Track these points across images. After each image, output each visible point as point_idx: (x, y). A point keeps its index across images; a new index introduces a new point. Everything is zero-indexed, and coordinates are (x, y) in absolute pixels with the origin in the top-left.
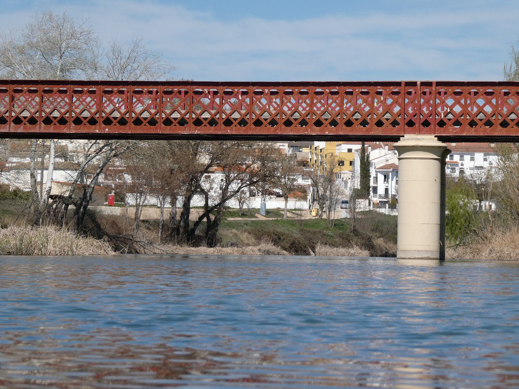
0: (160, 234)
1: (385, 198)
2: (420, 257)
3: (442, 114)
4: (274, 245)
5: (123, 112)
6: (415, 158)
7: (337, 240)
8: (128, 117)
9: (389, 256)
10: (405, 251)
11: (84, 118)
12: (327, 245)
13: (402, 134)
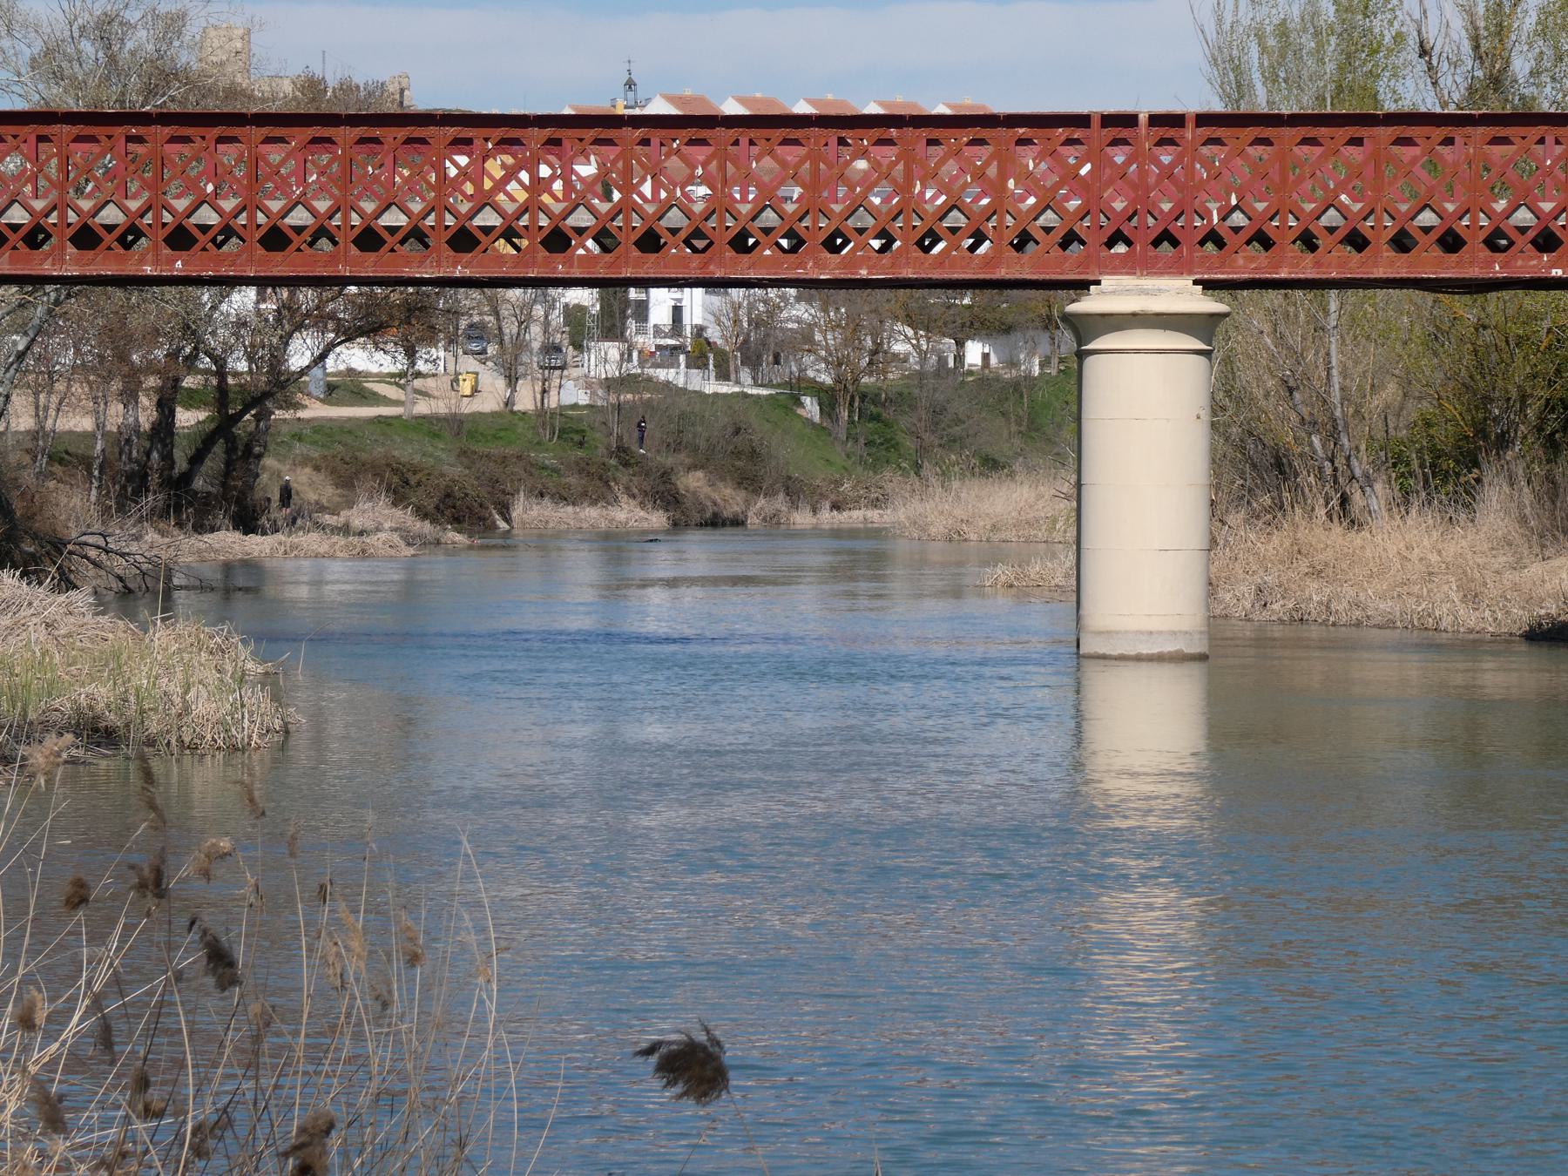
0: (94, 492)
2: (1155, 650)
3: (1215, 212)
4: (395, 504)
6: (1137, 351)
8: (244, 226)
9: (724, 524)
12: (547, 501)
13: (1093, 273)
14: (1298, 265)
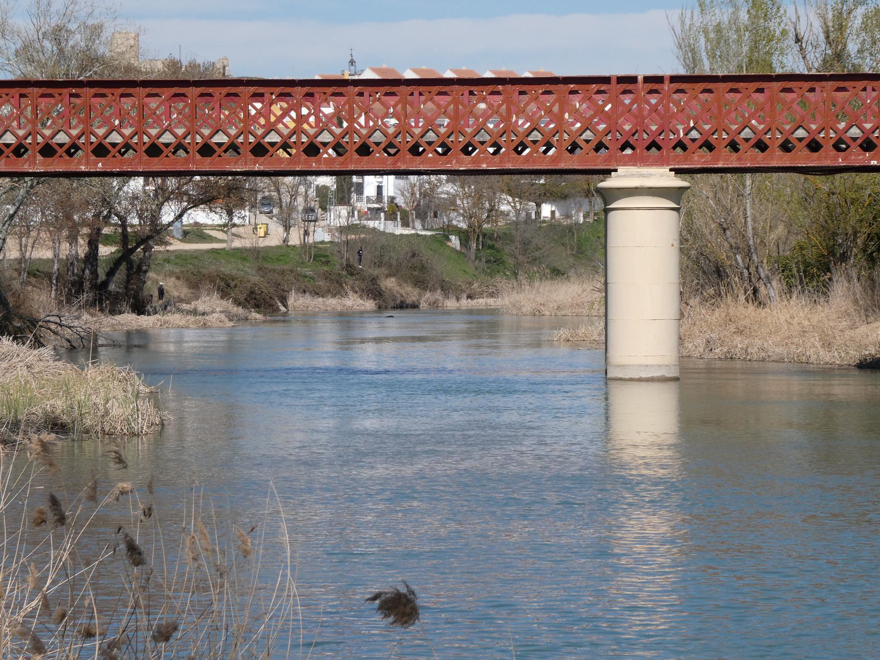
1: (376, 203)
3: (681, 131)
4: (222, 298)
5: (127, 135)
7: (321, 283)
8: (136, 143)
9: (407, 307)
10: (623, 366)
11: (58, 144)
12: (307, 294)
14: (728, 160)
